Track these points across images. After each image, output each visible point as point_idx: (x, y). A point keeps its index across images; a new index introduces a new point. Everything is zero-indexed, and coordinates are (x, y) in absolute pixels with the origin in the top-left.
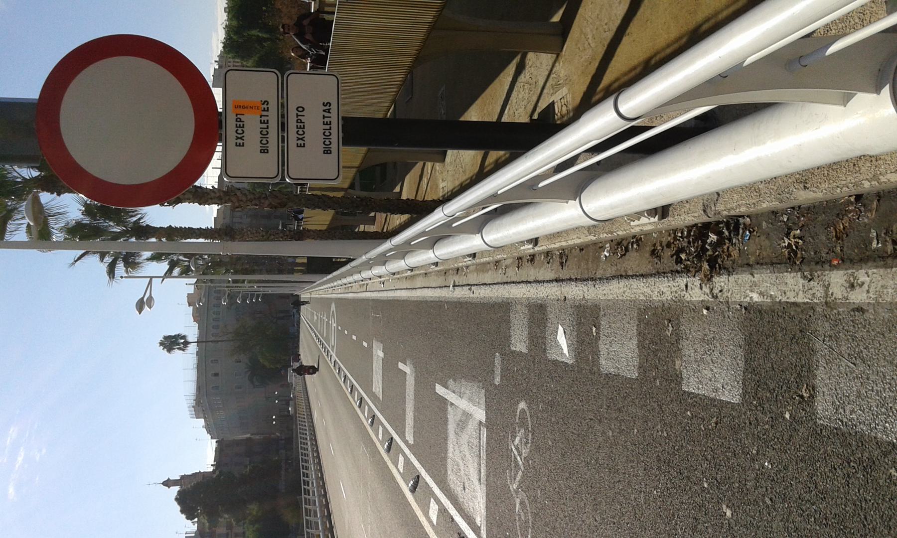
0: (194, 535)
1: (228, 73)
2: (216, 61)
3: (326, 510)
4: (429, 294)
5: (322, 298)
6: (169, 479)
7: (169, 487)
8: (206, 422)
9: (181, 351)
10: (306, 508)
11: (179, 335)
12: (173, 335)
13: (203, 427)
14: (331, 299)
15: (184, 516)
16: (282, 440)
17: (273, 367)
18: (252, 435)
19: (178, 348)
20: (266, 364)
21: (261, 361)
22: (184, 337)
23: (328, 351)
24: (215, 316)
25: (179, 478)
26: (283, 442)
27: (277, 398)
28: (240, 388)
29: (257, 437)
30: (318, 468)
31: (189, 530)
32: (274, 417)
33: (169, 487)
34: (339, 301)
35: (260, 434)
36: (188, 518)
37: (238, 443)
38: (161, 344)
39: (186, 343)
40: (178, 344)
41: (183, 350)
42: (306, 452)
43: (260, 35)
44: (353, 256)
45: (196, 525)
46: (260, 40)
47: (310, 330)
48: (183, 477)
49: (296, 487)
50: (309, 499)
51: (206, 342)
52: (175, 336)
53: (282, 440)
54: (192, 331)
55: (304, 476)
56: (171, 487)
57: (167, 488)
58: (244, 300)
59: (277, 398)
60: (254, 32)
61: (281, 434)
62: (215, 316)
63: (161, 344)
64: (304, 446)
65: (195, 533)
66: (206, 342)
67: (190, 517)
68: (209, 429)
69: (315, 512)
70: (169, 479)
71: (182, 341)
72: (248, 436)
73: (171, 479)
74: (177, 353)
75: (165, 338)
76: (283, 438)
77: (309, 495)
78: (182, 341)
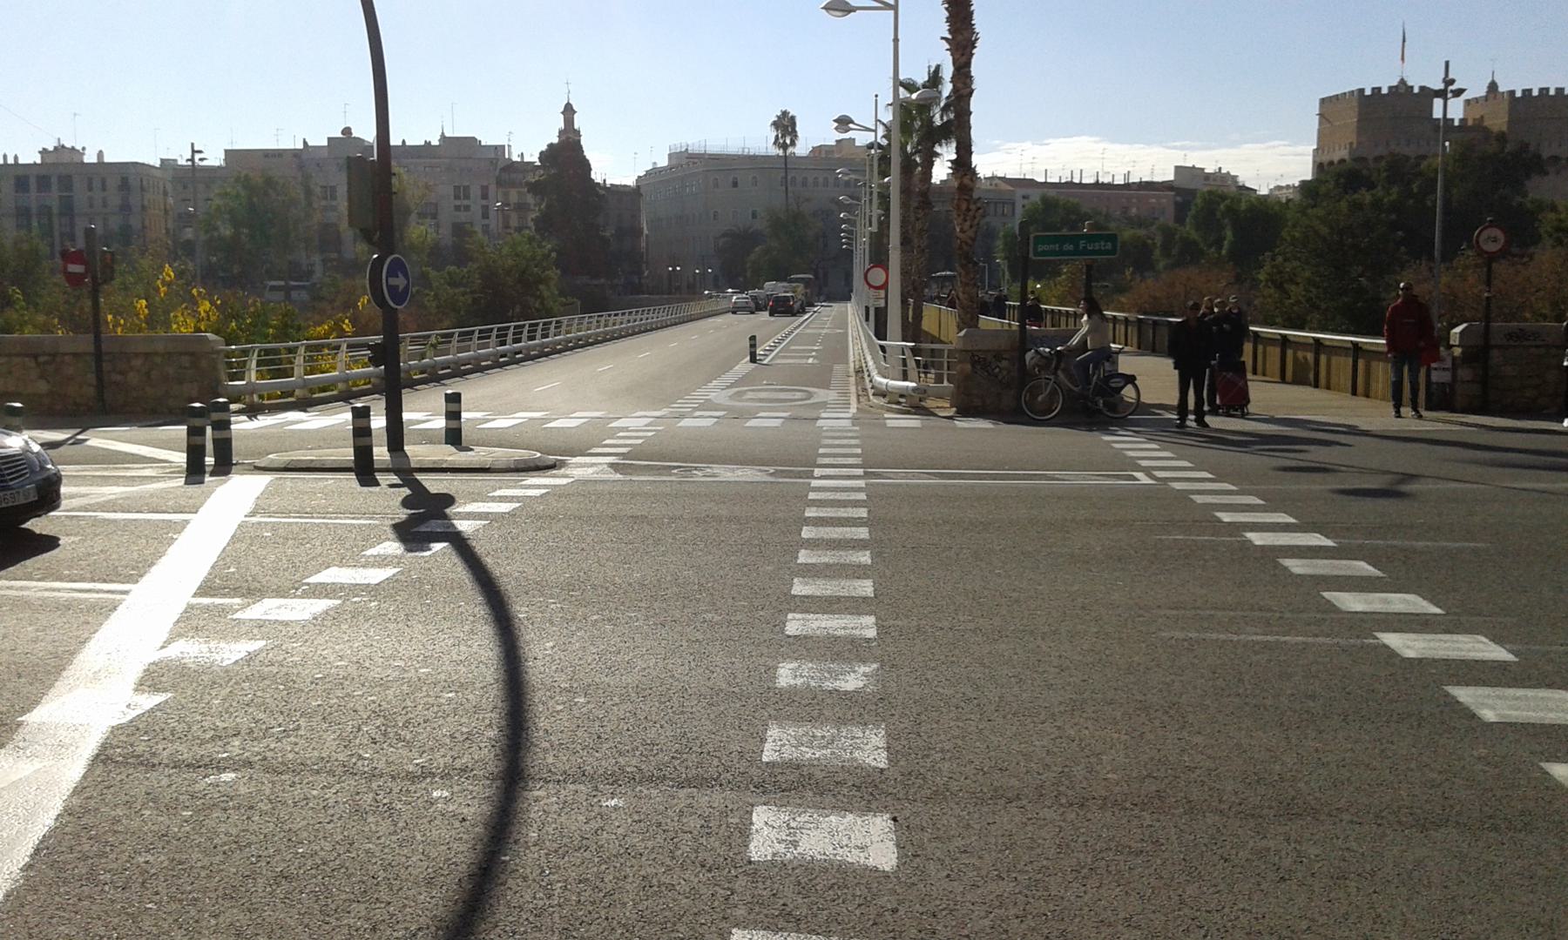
0: (507, 156)
1: (869, 280)
2: (1220, 169)
3: (489, 363)
4: (851, 353)
5: (847, 324)
6: (575, 112)
7: (562, 113)
8: (663, 169)
9: (773, 140)
10: (492, 330)
11: (796, 136)
12: (797, 129)
13: (655, 163)
14: (847, 329)
15: (544, 148)
16: (640, 279)
17: (748, 265)
18: (647, 236)
19: (777, 136)
20: (753, 257)
21: (757, 249)
22: (793, 143)
23: (772, 351)
24: (821, 180)
25: (576, 127)
26: (637, 281)
27: (674, 270)
28: (715, 219)
29: (643, 244)
30: (559, 347)
31: (513, 150)
32: (678, 268)
33: (562, 113)
34: (846, 334)
35: (647, 250)
36: (541, 153)
37: (635, 216)
38: (785, 113)
39: (784, 147)
40: (783, 136)
41: (775, 143)
42: (510, 337)
43: (1226, 242)
44: (955, 429)
45: (519, 160)
46: (1219, 243)
47: (786, 331)
48: (578, 133)
49: (595, 304)
50: (450, 342)
51: (786, 168)
52: (796, 132)
53: (640, 279)
54: (802, 148)
55: (530, 325)
56: (562, 116)
57: (562, 109)
58: (843, 221)
59: (674, 270)
60: (1229, 234)
61: (647, 277)
62: (821, 180)
63: (785, 113)
64: (585, 323)
65: (510, 159)
66: (786, 168)
67: (542, 155)
68: (654, 173)
69: (486, 346)
70: (575, 112)
71: (788, 141)
72: (646, 232)
73: (576, 116)
74: (772, 134)
75: (793, 118)
76: (643, 281)
77: (479, 338)
78: (788, 141)
